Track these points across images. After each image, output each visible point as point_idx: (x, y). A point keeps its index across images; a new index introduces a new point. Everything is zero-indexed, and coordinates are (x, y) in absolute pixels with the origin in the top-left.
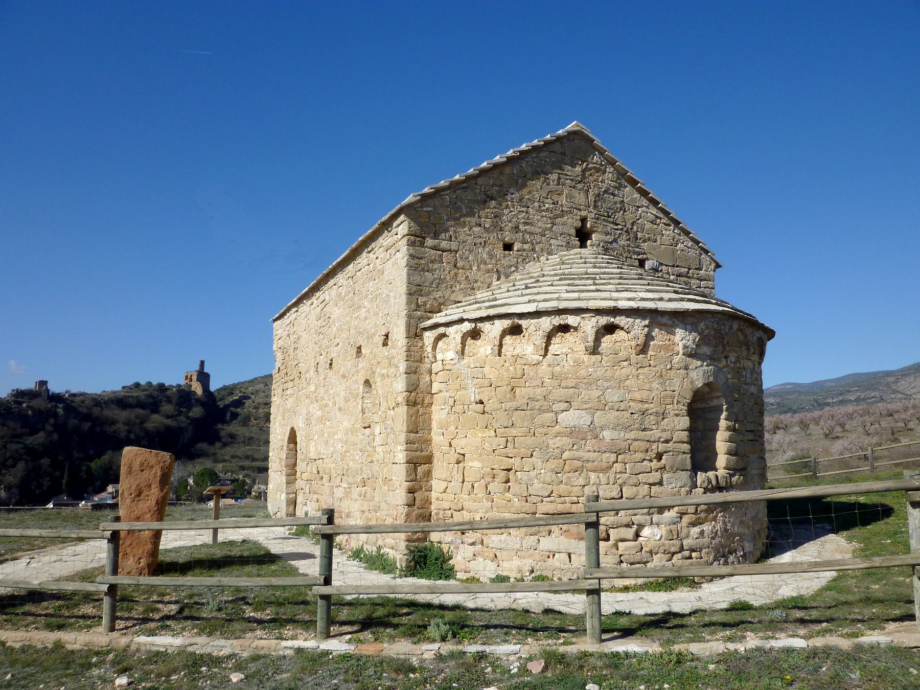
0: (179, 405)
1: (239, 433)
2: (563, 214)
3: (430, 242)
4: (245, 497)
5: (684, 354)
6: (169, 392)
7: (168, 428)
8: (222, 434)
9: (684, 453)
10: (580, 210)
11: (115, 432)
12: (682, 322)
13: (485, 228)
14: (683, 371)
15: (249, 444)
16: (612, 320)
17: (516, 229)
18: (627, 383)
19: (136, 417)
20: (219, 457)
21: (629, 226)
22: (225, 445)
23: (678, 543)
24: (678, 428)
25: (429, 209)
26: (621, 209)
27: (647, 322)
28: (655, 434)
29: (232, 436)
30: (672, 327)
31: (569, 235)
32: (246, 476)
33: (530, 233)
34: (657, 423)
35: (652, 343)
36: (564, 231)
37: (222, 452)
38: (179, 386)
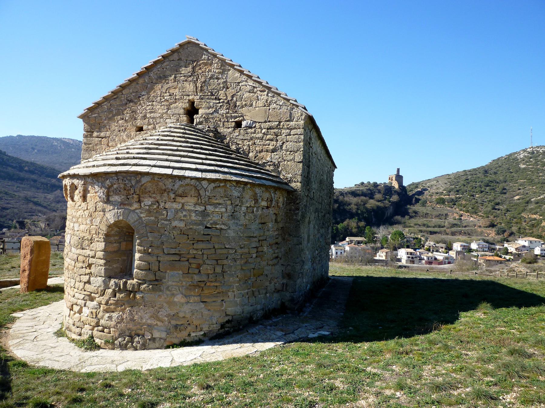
0: (385, 194)
1: (419, 211)
3: (95, 134)
4: (421, 248)
6: (379, 187)
7: (378, 207)
8: (410, 211)
10: (189, 96)
11: (350, 209)
13: (126, 120)
14: (102, 213)
15: (426, 217)
17: (145, 117)
19: (362, 201)
20: (407, 224)
21: (229, 98)
22: (411, 217)
23: (96, 320)
24: (98, 250)
25: (95, 115)
26: (224, 87)
28: (88, 252)
29: (416, 212)
31: (179, 114)
32: (423, 236)
33: (153, 118)
35: (88, 195)
36: (176, 112)
37: (409, 221)
38: (385, 183)
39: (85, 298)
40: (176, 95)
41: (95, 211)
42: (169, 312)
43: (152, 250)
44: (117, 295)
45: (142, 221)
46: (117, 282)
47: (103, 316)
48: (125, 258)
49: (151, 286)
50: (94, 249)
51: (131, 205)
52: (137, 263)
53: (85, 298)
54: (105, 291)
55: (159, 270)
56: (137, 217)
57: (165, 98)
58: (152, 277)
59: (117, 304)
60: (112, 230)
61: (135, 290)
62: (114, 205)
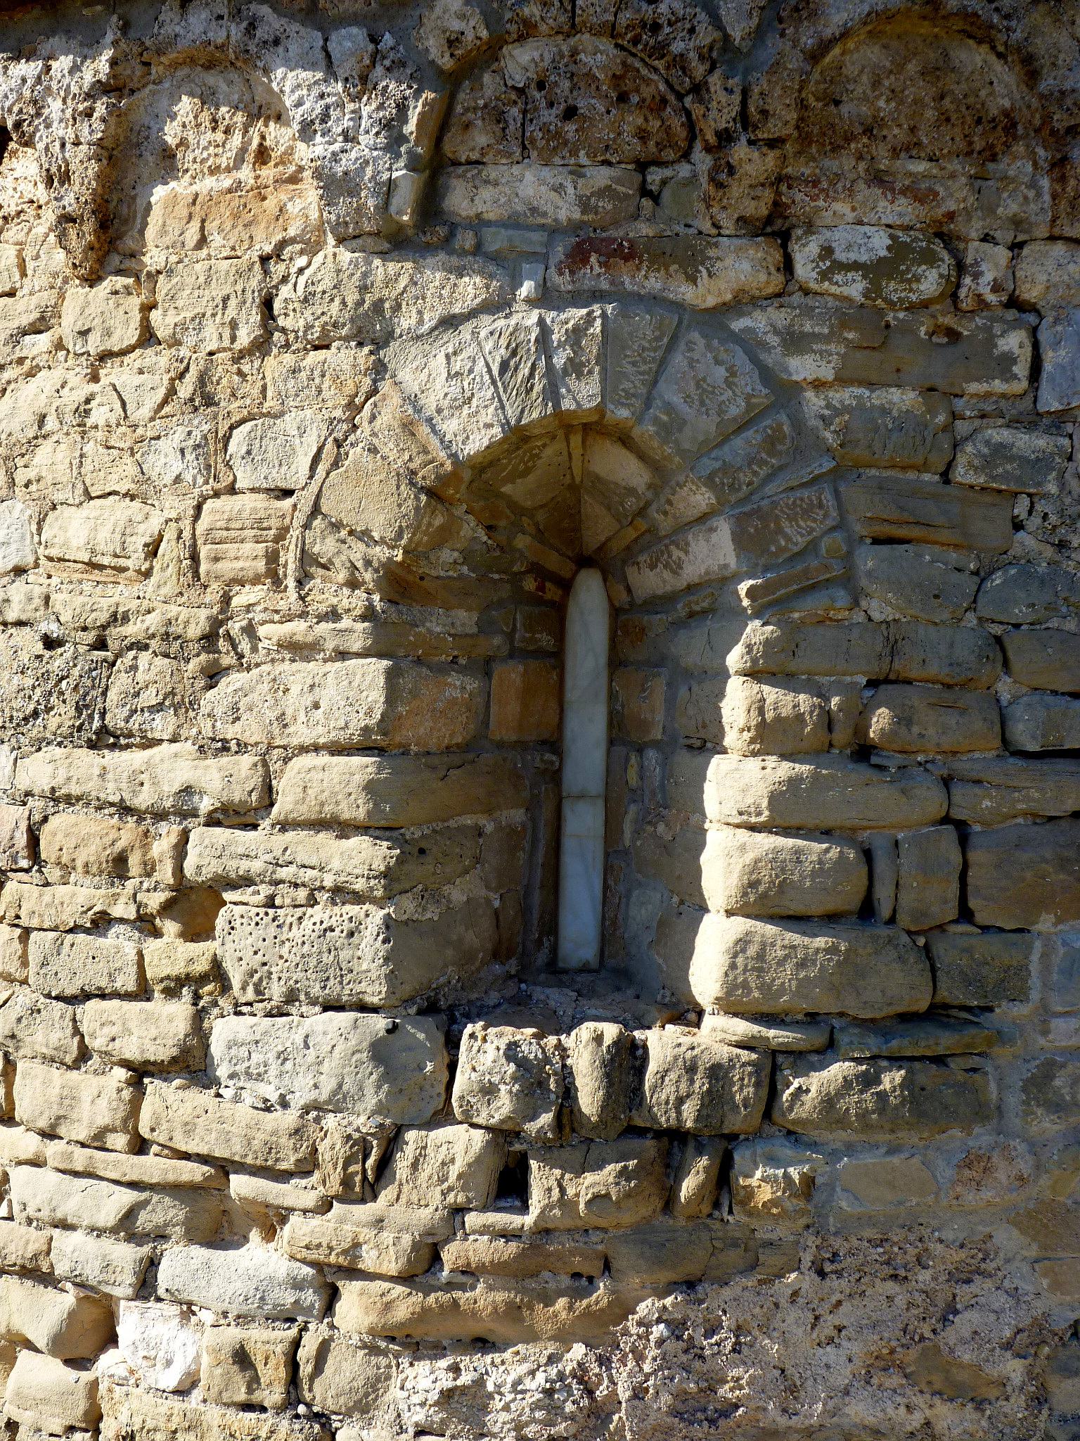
9: (341, 894)
14: (345, 358)
24: (301, 734)
27: (101, 66)
28: (168, 768)
34: (179, 703)
39: (145, 1220)
41: (261, 346)
42: (1039, 1307)
43: (903, 719)
44: (541, 1180)
45: (798, 424)
46: (530, 1050)
47: (376, 1384)
48: (517, 815)
49: (891, 1079)
50: (250, 729)
51: (689, 257)
52: (723, 862)
53: (145, 1220)
54: (392, 1142)
55: (966, 914)
56: (749, 382)
58: (897, 985)
59: (538, 1266)
60: (443, 537)
61: (734, 1123)
62: (505, 265)
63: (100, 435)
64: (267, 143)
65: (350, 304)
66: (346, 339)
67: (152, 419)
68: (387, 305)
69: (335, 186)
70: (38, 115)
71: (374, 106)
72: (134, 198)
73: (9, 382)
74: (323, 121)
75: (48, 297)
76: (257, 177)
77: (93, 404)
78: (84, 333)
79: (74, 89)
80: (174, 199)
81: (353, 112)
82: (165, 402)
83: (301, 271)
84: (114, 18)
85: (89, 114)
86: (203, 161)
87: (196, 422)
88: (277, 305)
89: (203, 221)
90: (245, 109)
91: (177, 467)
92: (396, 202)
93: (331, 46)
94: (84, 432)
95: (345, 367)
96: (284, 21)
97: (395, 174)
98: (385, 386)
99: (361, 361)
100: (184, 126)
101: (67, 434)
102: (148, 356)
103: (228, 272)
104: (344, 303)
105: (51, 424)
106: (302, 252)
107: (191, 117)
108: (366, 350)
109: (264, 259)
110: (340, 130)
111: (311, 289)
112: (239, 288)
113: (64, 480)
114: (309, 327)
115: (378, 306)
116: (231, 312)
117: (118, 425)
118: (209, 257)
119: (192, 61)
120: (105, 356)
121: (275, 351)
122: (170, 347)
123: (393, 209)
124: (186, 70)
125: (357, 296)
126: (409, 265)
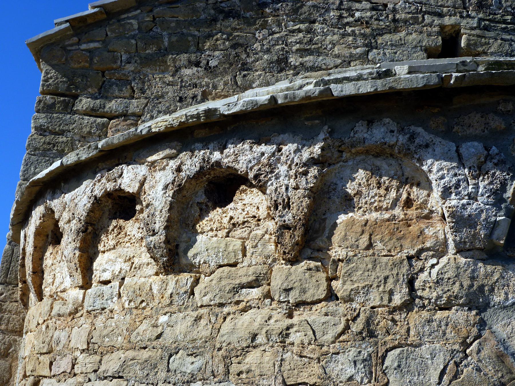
2: (396, 25)
3: (84, 103)
5: (459, 251)
10: (441, 15)
12: (447, 134)
14: (459, 315)
16: (216, 156)
18: (252, 358)
25: (92, 45)
27: (317, 149)
30: (408, 153)
40: (394, 11)
41: (408, 306)
57: (357, 14)
63: (295, 349)
64: (412, 197)
65: (465, 287)
66: (462, 305)
67: (333, 342)
68: (486, 288)
69: (460, 221)
70: (272, 172)
71: (486, 182)
72: (324, 220)
73: (229, 314)
74: (456, 188)
75: (262, 269)
76: (405, 214)
77: (291, 331)
78: (287, 291)
79: (296, 160)
80: (352, 223)
81: (474, 184)
82: (343, 333)
83: (433, 266)
84: (326, 127)
85: (305, 173)
86: (371, 203)
87: (364, 346)
88: (417, 284)
89: (371, 235)
90: (398, 179)
91: (350, 371)
92: (497, 233)
93: (462, 150)
94: (284, 347)
95: (460, 321)
96: (432, 136)
97: (498, 219)
98: (486, 334)
99: (472, 318)
100: (360, 184)
101: (272, 347)
102: (332, 306)
103: (387, 264)
104: (462, 285)
105: (261, 339)
106: (433, 256)
107: (364, 180)
108: (474, 312)
109: (410, 258)
110: (466, 193)
111: (440, 276)
112: (395, 272)
113: (269, 373)
114: (439, 297)
115: (481, 288)
116: (390, 285)
117: (310, 344)
118: (374, 254)
119: (367, 152)
120: (299, 304)
121: (416, 309)
122: (345, 302)
123: (495, 237)
124: (363, 157)
125: (469, 282)
126: (500, 267)
